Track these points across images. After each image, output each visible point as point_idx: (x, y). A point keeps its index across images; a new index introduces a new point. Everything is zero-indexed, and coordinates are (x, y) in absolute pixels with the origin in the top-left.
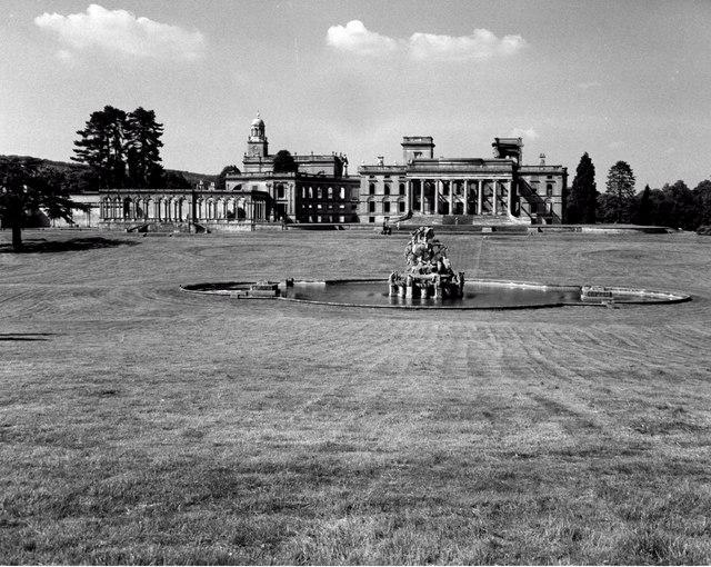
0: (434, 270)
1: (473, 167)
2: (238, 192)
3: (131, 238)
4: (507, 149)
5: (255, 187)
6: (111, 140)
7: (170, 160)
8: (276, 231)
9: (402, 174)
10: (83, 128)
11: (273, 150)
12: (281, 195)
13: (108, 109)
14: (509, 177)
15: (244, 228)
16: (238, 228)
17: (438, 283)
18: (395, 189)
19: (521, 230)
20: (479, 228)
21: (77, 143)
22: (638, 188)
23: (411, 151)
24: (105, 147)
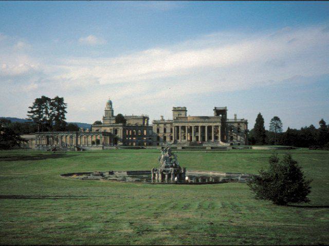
0: (172, 166)
1: (202, 120)
2: (97, 132)
3: (74, 154)
4: (221, 112)
5: (105, 130)
6: (44, 110)
7: (69, 118)
8: (113, 149)
9: (171, 124)
10: (32, 105)
11: (115, 114)
12: (116, 133)
13: (43, 97)
14: (219, 124)
15: (99, 148)
16: (96, 149)
17: (172, 172)
18: (168, 131)
19: (224, 148)
20: (205, 148)
21: (29, 112)
22: (284, 130)
23: (176, 113)
24: (42, 114)
